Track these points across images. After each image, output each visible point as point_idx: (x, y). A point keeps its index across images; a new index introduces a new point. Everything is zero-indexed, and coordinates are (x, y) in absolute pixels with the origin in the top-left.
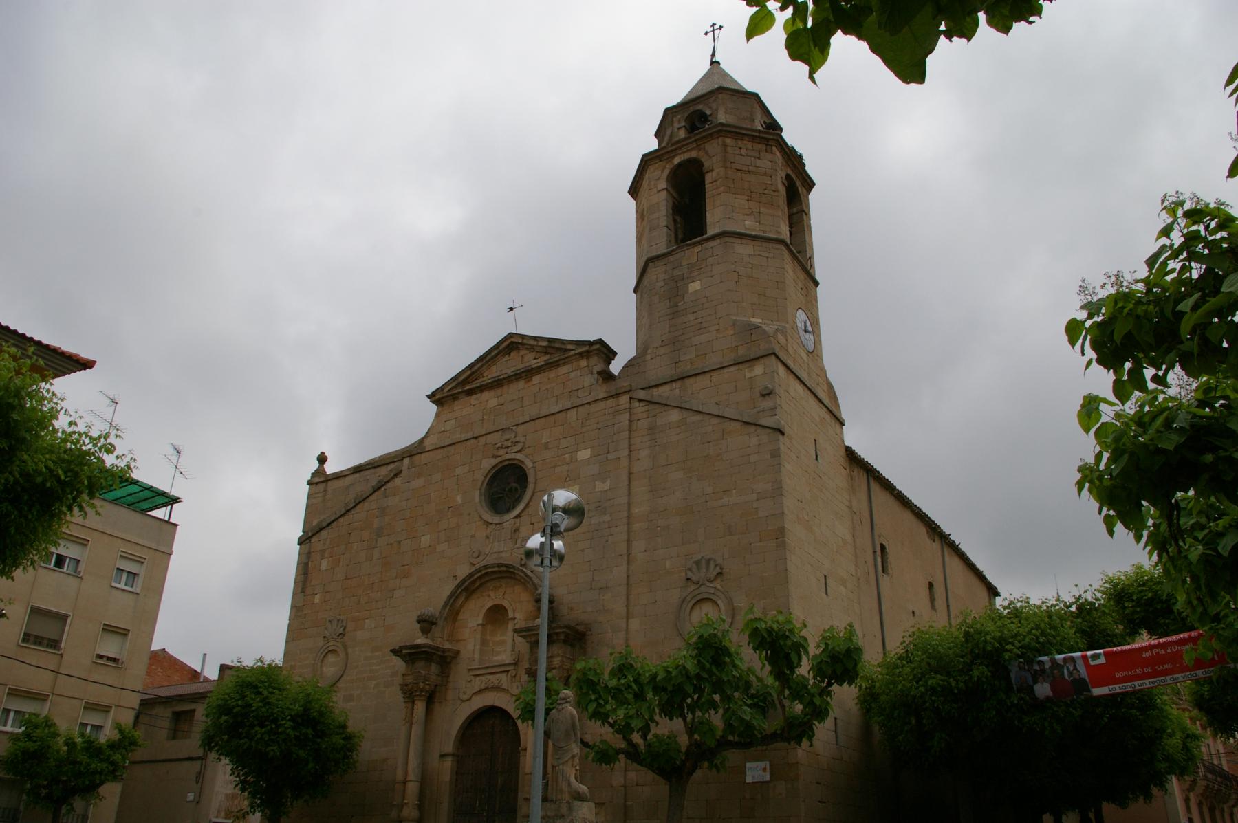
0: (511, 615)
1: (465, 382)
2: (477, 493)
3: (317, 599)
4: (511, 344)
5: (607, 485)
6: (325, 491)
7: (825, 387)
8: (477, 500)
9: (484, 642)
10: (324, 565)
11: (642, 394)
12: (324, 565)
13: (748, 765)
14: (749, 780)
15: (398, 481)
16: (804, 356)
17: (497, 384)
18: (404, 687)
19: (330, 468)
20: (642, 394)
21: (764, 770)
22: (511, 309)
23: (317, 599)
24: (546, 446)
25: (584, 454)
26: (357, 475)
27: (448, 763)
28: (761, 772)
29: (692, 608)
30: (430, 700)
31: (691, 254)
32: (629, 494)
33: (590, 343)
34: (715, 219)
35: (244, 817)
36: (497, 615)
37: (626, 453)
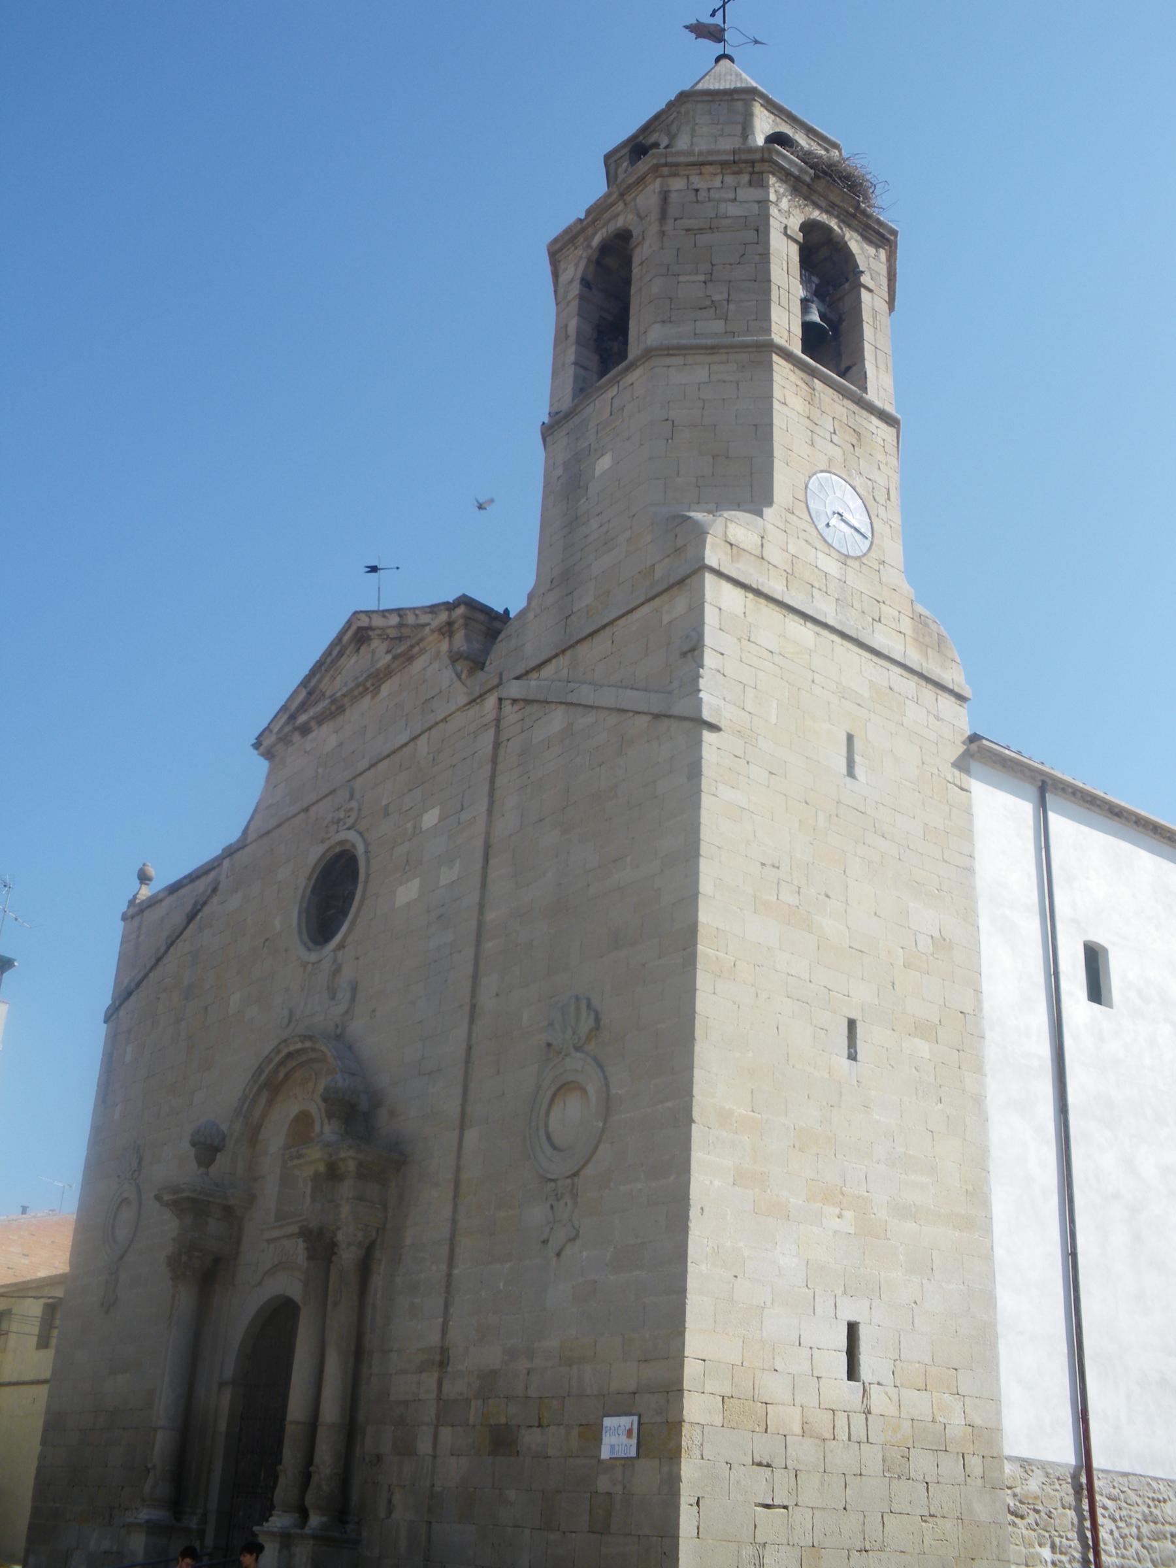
1: (303, 707)
4: (357, 634)
11: (514, 689)
14: (605, 1454)
20: (514, 689)
22: (374, 569)
26: (175, 896)
27: (226, 1398)
28: (624, 1439)
29: (554, 1096)
33: (450, 607)
34: (646, 331)
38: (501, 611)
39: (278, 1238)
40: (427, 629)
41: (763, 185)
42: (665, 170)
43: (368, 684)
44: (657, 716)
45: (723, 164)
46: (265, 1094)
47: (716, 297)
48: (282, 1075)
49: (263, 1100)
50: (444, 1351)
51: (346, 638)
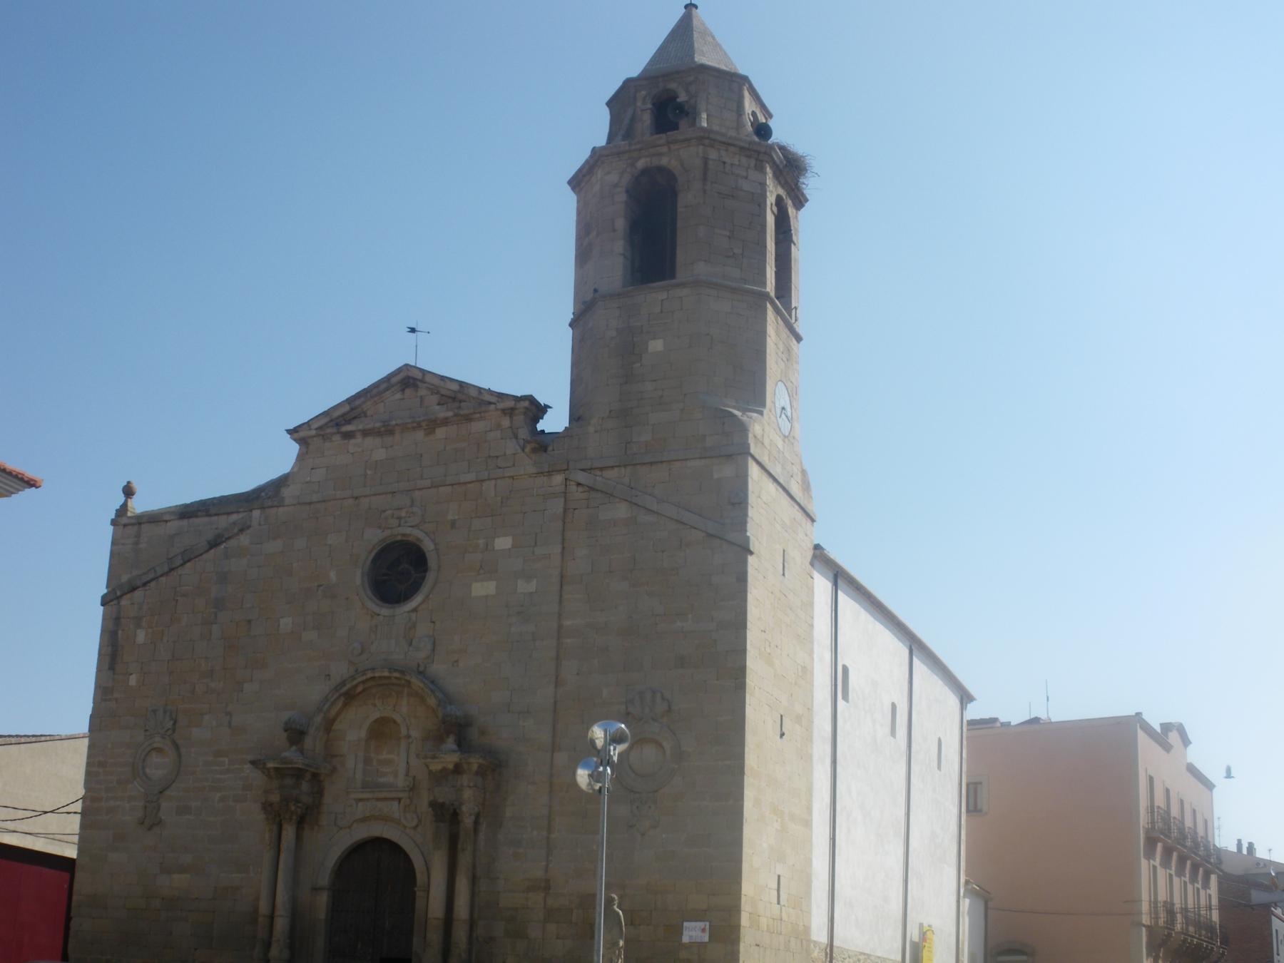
0: (404, 732)
2: (358, 573)
3: (133, 680)
5: (532, 586)
6: (138, 536)
7: (799, 478)
8: (358, 581)
9: (367, 761)
10: (141, 637)
11: (582, 477)
12: (141, 637)
13: (685, 924)
14: (685, 939)
15: (244, 540)
16: (780, 444)
17: (385, 431)
18: (267, 807)
19: (139, 506)
20: (582, 477)
21: (703, 930)
22: (413, 330)
23: (133, 680)
24: (453, 524)
25: (503, 543)
26: (185, 522)
27: (323, 899)
28: (700, 933)
30: (301, 823)
31: (654, 298)
32: (560, 602)
35: (350, 827)
36: (381, 731)
37: (558, 549)
38: (1233, 848)
39: (368, 799)
40: (492, 407)
41: (762, 170)
42: (707, 142)
43: (424, 424)
44: (710, 535)
45: (742, 148)
46: (342, 699)
47: (736, 251)
48: (360, 689)
49: (340, 704)
50: (547, 881)
51: (394, 380)
